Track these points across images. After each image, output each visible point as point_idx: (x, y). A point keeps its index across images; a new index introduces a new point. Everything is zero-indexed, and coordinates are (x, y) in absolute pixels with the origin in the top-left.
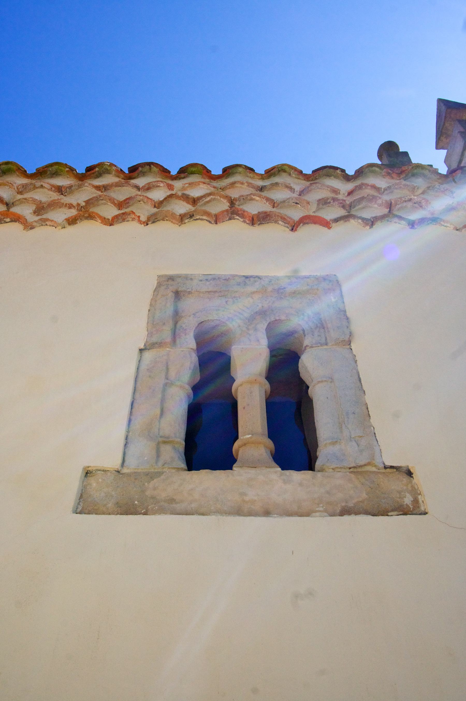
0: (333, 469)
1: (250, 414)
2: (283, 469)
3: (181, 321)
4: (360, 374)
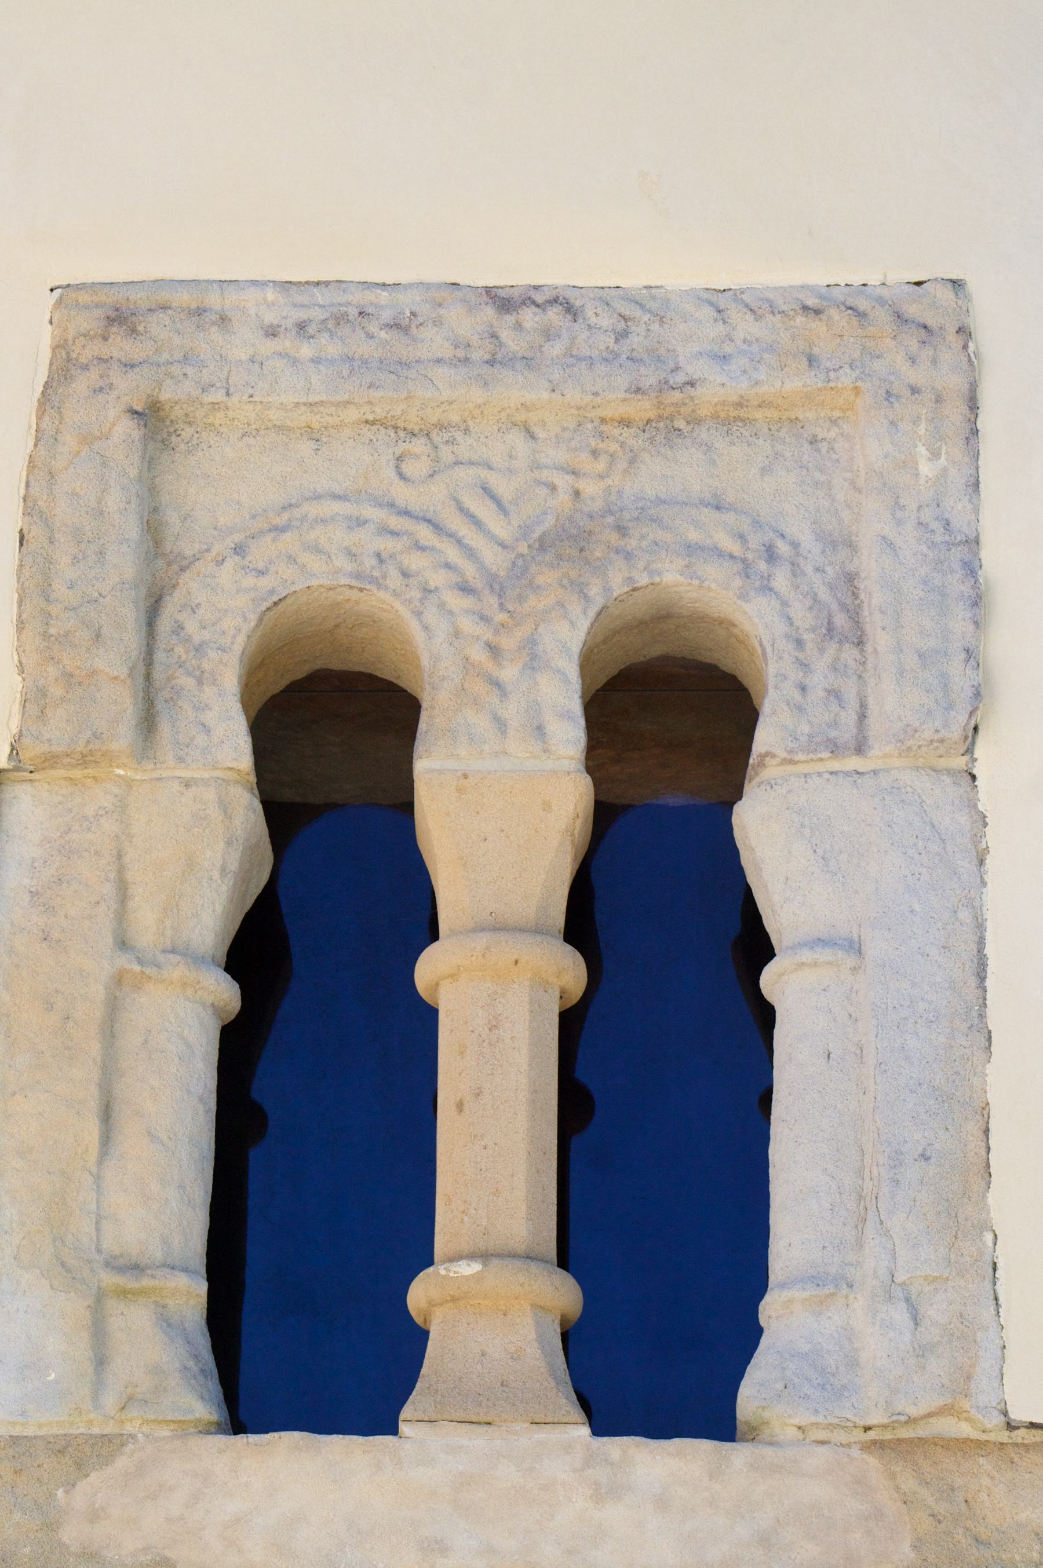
0: (800, 1428)
1: (483, 1143)
2: (599, 1429)
3: (177, 594)
4: (989, 935)
